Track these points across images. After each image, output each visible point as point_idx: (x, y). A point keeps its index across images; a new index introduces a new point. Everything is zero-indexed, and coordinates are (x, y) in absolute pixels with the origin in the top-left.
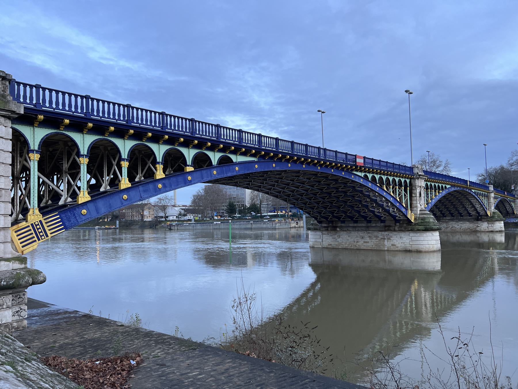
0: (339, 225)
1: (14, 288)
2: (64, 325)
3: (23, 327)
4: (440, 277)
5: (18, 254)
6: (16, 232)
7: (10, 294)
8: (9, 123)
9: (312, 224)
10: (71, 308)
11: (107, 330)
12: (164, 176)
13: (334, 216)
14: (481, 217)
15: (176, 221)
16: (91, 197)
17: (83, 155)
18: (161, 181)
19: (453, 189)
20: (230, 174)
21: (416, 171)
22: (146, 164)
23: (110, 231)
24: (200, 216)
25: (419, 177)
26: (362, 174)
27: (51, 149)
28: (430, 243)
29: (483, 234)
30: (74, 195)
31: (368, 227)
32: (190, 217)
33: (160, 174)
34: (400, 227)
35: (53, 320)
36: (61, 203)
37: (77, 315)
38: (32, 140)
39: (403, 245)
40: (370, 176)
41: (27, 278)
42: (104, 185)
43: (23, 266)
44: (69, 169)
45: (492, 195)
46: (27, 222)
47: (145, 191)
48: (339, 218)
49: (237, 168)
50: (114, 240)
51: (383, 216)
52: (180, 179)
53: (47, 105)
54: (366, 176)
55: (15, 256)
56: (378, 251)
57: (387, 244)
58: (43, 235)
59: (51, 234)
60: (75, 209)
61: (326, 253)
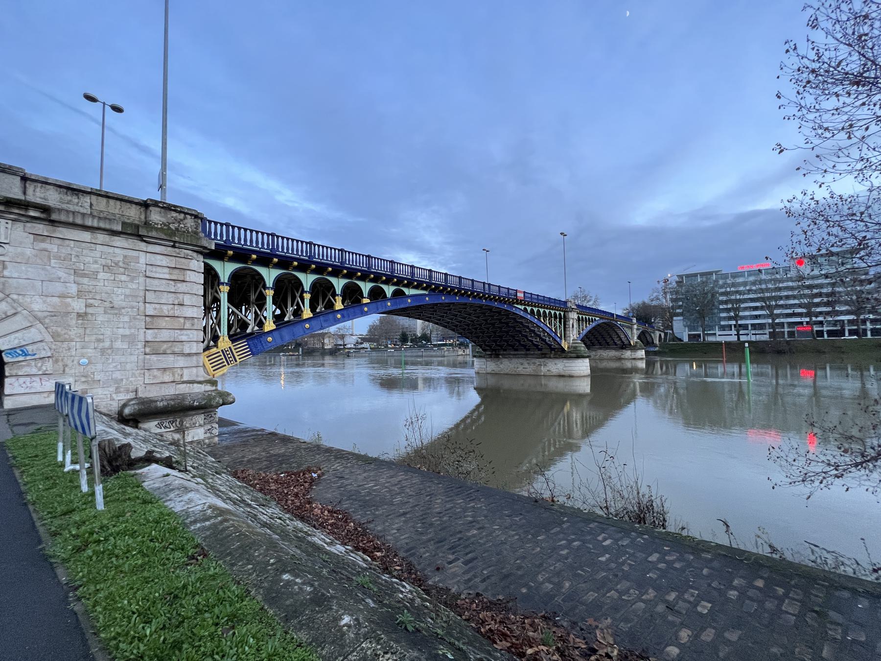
0: (502, 353)
1: (206, 408)
4: (589, 398)
8: (201, 258)
9: (478, 352)
13: (497, 345)
14: (625, 346)
16: (277, 326)
19: (602, 321)
20: (402, 306)
21: (569, 305)
24: (375, 344)
26: (522, 307)
27: (239, 282)
28: (581, 368)
30: (261, 324)
33: (339, 305)
34: (555, 354)
36: (249, 331)
39: (557, 370)
43: (214, 388)
44: (257, 300)
45: (635, 327)
47: (326, 321)
50: (298, 365)
52: (357, 310)
54: (525, 309)
56: (536, 376)
57: (544, 370)
61: (489, 377)
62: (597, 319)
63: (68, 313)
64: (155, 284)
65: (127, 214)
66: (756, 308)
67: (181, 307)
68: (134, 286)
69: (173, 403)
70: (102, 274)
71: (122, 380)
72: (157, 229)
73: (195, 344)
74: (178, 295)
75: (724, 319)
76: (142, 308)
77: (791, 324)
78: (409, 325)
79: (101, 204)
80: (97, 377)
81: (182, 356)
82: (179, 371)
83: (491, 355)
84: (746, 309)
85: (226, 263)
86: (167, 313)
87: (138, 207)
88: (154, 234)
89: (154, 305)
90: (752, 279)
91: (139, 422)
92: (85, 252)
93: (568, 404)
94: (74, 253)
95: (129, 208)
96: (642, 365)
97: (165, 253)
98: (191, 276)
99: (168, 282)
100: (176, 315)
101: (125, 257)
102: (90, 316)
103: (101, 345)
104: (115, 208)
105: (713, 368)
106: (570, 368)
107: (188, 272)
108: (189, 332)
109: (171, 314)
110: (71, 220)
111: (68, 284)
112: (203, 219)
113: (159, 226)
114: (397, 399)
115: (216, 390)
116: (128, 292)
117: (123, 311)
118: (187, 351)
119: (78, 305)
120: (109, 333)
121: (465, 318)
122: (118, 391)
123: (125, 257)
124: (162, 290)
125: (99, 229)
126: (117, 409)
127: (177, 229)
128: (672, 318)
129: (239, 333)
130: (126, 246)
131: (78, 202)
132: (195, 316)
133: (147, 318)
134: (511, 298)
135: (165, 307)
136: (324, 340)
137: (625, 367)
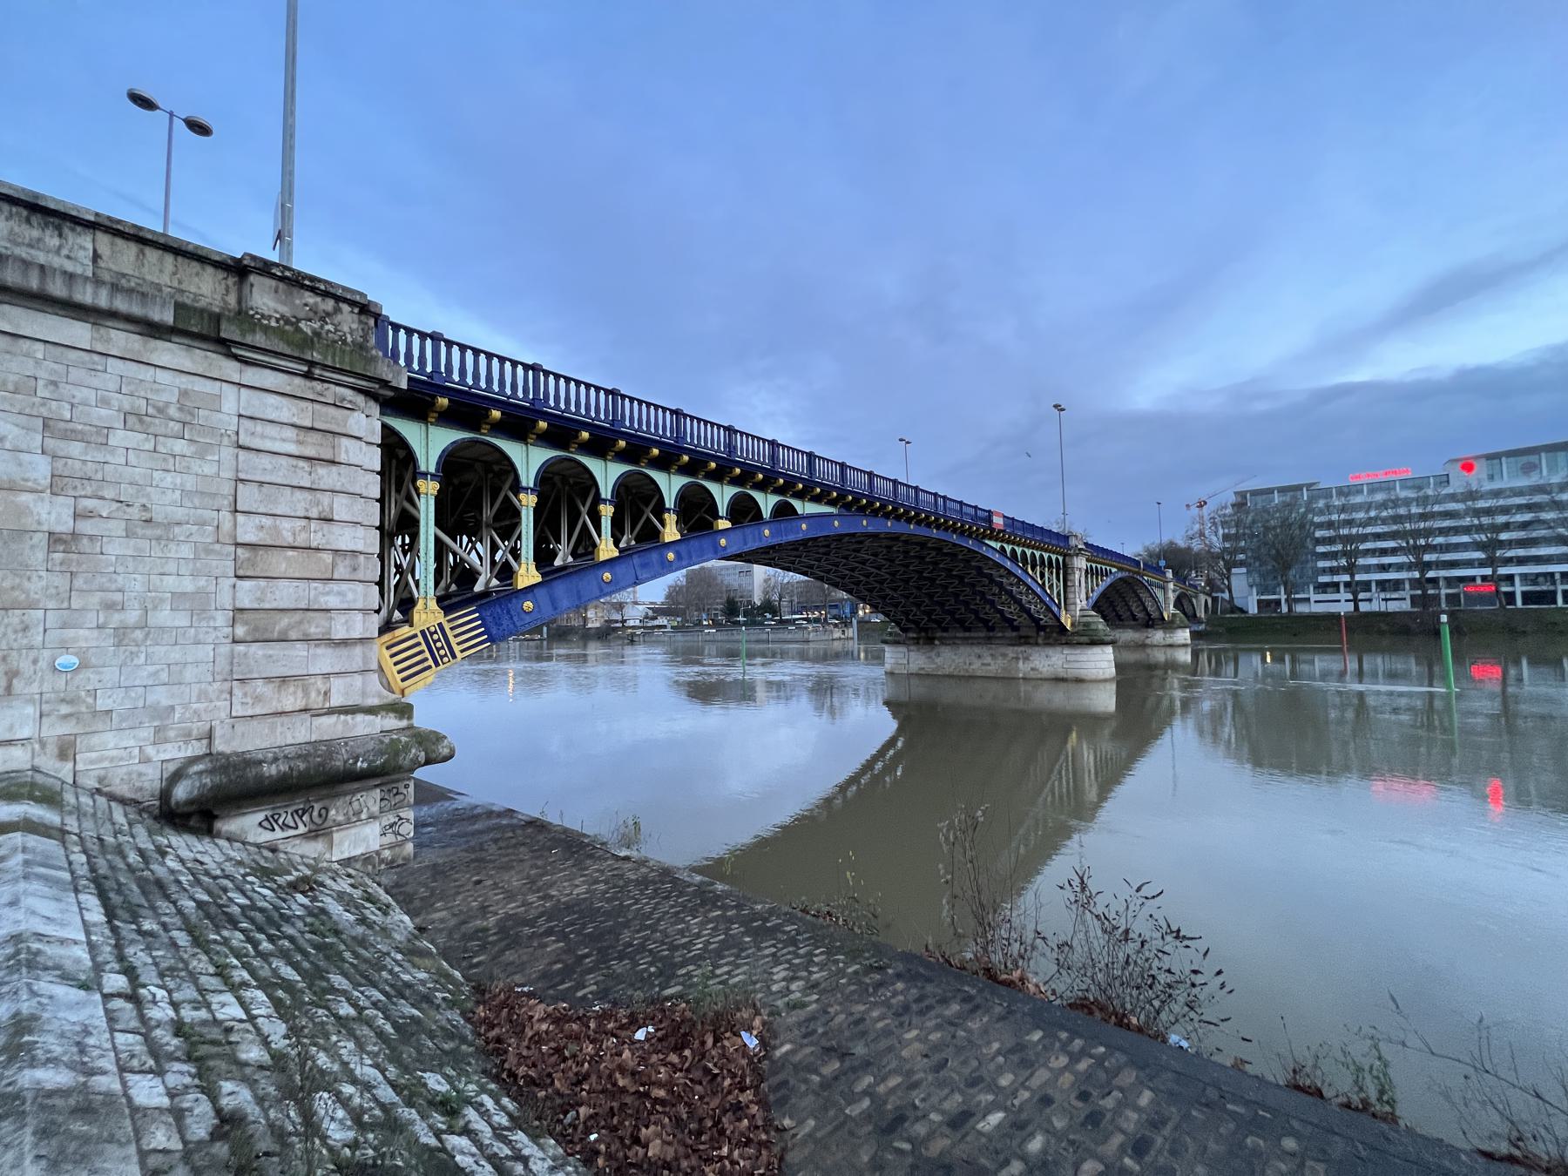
0: (938, 634)
1: (387, 774)
2: (493, 848)
3: (404, 859)
4: (1114, 724)
5: (394, 696)
6: (388, 648)
7: (376, 786)
8: (375, 409)
9: (891, 634)
10: (501, 803)
11: (597, 871)
12: (616, 554)
13: (930, 620)
14: (1152, 621)
15: (639, 628)
16: (543, 575)
17: (527, 489)
18: (673, 547)
19: (1120, 575)
20: (791, 538)
21: (1073, 542)
22: (642, 513)
23: (531, 643)
24: (679, 619)
25: (1079, 552)
27: (456, 481)
28: (1099, 665)
29: (1156, 649)
30: (505, 573)
31: (989, 638)
32: (662, 621)
33: (671, 533)
34: (1046, 638)
35: (465, 835)
36: (478, 588)
37: (515, 821)
38: (424, 451)
40: (1008, 548)
41: (413, 751)
42: (561, 555)
43: (404, 723)
44: (497, 518)
45: (1171, 586)
46: (411, 626)
47: (644, 566)
48: (938, 623)
49: (804, 526)
50: (539, 658)
51: (1022, 620)
52: (706, 543)
53: (456, 377)
54: (1002, 547)
55: (385, 701)
56: (1008, 680)
57: (1023, 668)
58: (446, 655)
59: (462, 651)
60: (510, 600)
61: (914, 681)
62: (1114, 570)
63: (21, 533)
64: (259, 467)
65: (193, 289)
66: (1384, 552)
67: (325, 526)
68: (209, 469)
69: (302, 766)
70: (121, 433)
71: (172, 708)
72: (266, 329)
73: (359, 616)
74: (319, 495)
75: (1324, 571)
76: (227, 526)
77: (1450, 581)
78: (740, 586)
79: (124, 258)
80: (102, 704)
81: (329, 645)
82: (320, 683)
83: (918, 639)
84: (1367, 552)
85: (432, 429)
86: (290, 540)
87: (221, 275)
88: (259, 339)
89: (257, 519)
90: (1379, 497)
91: (216, 817)
92: (76, 374)
93: (1074, 735)
94: (41, 374)
95: (197, 274)
96: (1185, 657)
97: (288, 390)
98: (349, 451)
99: (294, 461)
100: (314, 545)
101: (184, 393)
102: (85, 541)
103: (116, 619)
104: (159, 270)
105: (1305, 662)
106: (1077, 665)
107: (345, 441)
108: (344, 586)
109: (300, 542)
110: (34, 283)
111: (25, 457)
112: (377, 316)
113: (273, 324)
114: (714, 718)
115: (410, 727)
116: (190, 483)
117: (177, 530)
118: (339, 633)
119: (55, 514)
120: (138, 587)
121: (853, 570)
122: (160, 738)
123: (184, 393)
124: (279, 481)
125: (113, 315)
126: (157, 785)
127: (317, 334)
128: (1229, 570)
129: (454, 595)
130: (187, 365)
131: (60, 247)
132: (360, 547)
133: (240, 551)
134: (980, 524)
135: (286, 525)
136: (586, 612)
137: (1152, 661)
